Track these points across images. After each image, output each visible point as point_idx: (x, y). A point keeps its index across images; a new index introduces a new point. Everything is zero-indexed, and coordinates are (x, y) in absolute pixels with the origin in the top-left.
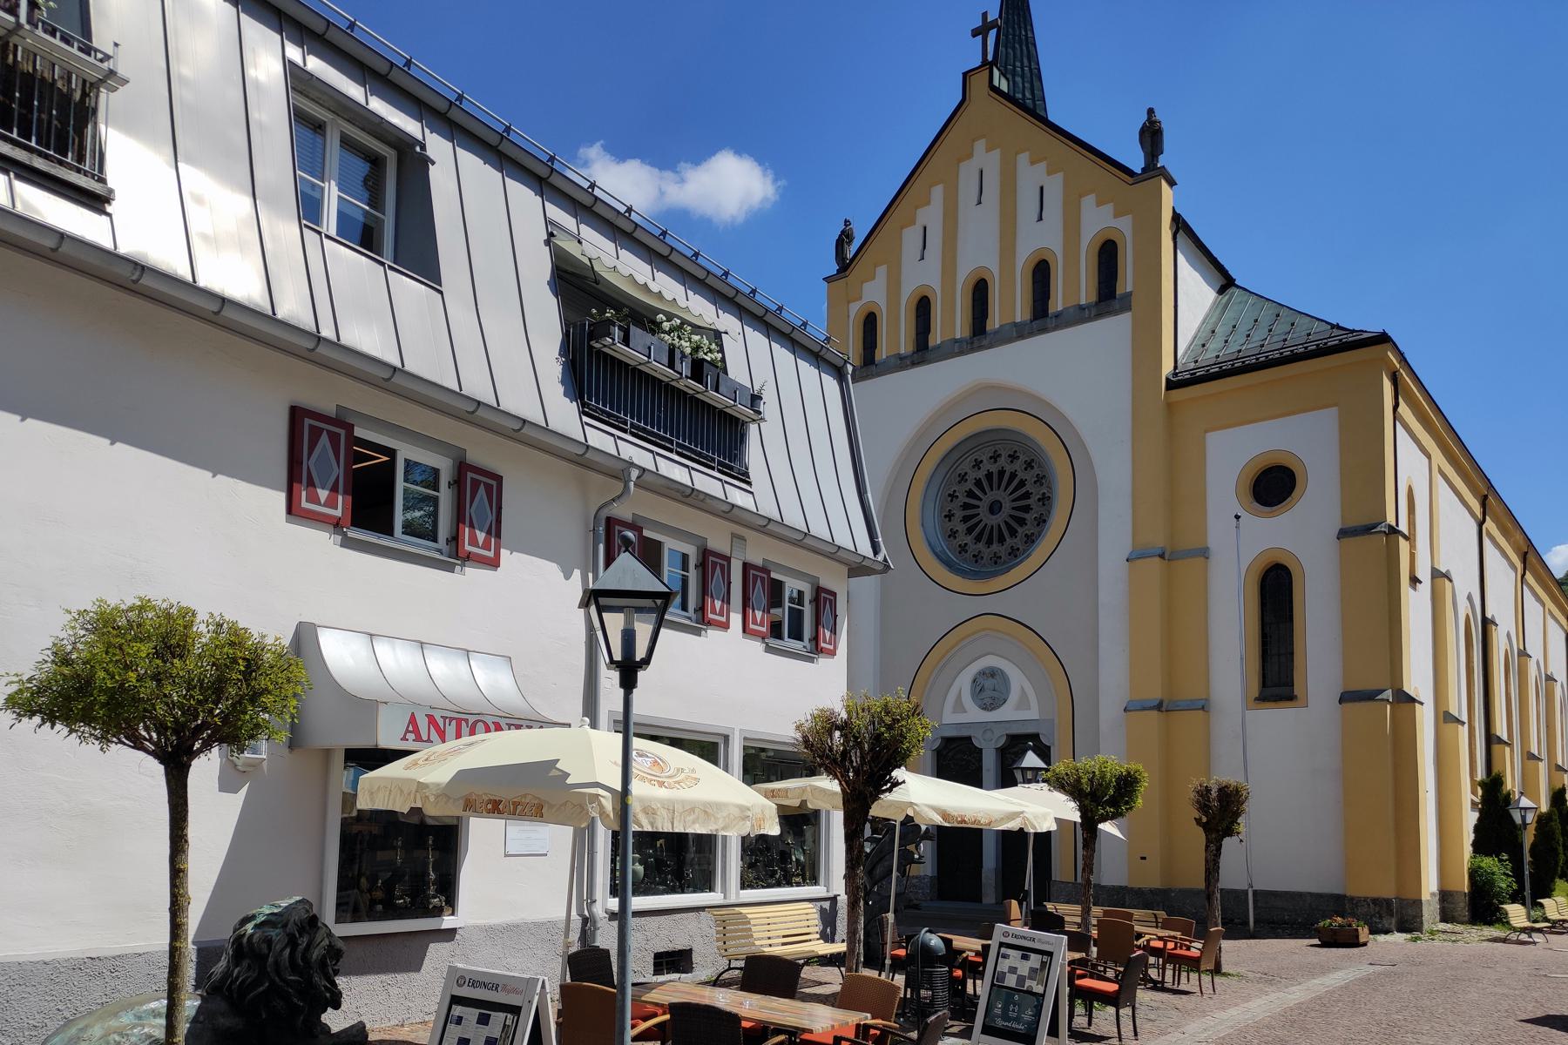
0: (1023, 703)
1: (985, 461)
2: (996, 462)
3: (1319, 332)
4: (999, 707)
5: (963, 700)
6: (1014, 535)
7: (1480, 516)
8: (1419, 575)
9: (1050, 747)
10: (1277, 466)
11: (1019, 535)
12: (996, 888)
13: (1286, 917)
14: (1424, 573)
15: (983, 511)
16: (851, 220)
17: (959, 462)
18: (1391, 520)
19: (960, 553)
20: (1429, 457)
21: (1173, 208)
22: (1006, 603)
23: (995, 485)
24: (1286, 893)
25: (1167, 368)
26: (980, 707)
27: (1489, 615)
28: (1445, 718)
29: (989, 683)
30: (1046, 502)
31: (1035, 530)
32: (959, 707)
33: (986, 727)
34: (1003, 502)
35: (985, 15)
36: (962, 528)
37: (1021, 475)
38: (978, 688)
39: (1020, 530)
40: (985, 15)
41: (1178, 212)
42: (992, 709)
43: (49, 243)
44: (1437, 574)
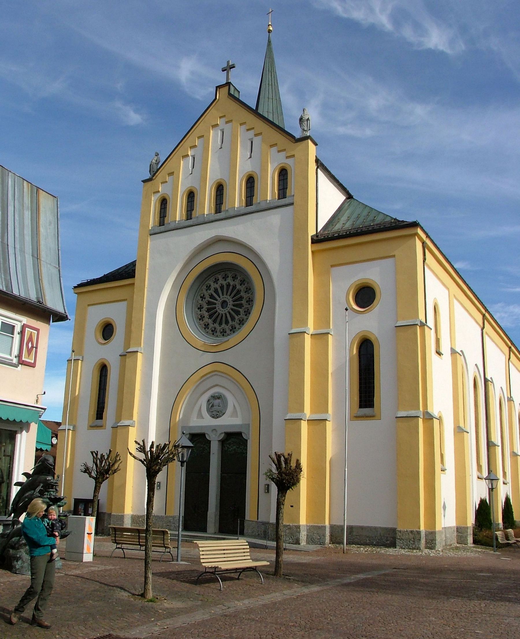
0: (235, 414)
1: (220, 279)
2: (225, 280)
3: (379, 219)
4: (221, 416)
5: (203, 413)
6: (222, 286)
7: (481, 323)
8: (442, 350)
9: (247, 440)
10: (374, 291)
11: (236, 320)
12: (215, 523)
13: (368, 541)
14: (445, 349)
15: (218, 307)
16: (158, 153)
17: (233, 380)
18: (422, 317)
19: (205, 329)
20: (448, 289)
21: (316, 156)
22: (227, 357)
23: (225, 293)
24: (368, 527)
25: (312, 232)
26: (211, 416)
27: (488, 377)
28: (459, 431)
29: (217, 402)
30: (251, 303)
31: (245, 317)
32: (200, 415)
33: (214, 429)
34: (228, 301)
35: (228, 62)
36: (206, 314)
37: (242, 294)
38: (210, 407)
39: (236, 317)
40: (228, 62)
41: (318, 158)
42: (218, 418)
43: (165, 207)
44: (453, 352)
